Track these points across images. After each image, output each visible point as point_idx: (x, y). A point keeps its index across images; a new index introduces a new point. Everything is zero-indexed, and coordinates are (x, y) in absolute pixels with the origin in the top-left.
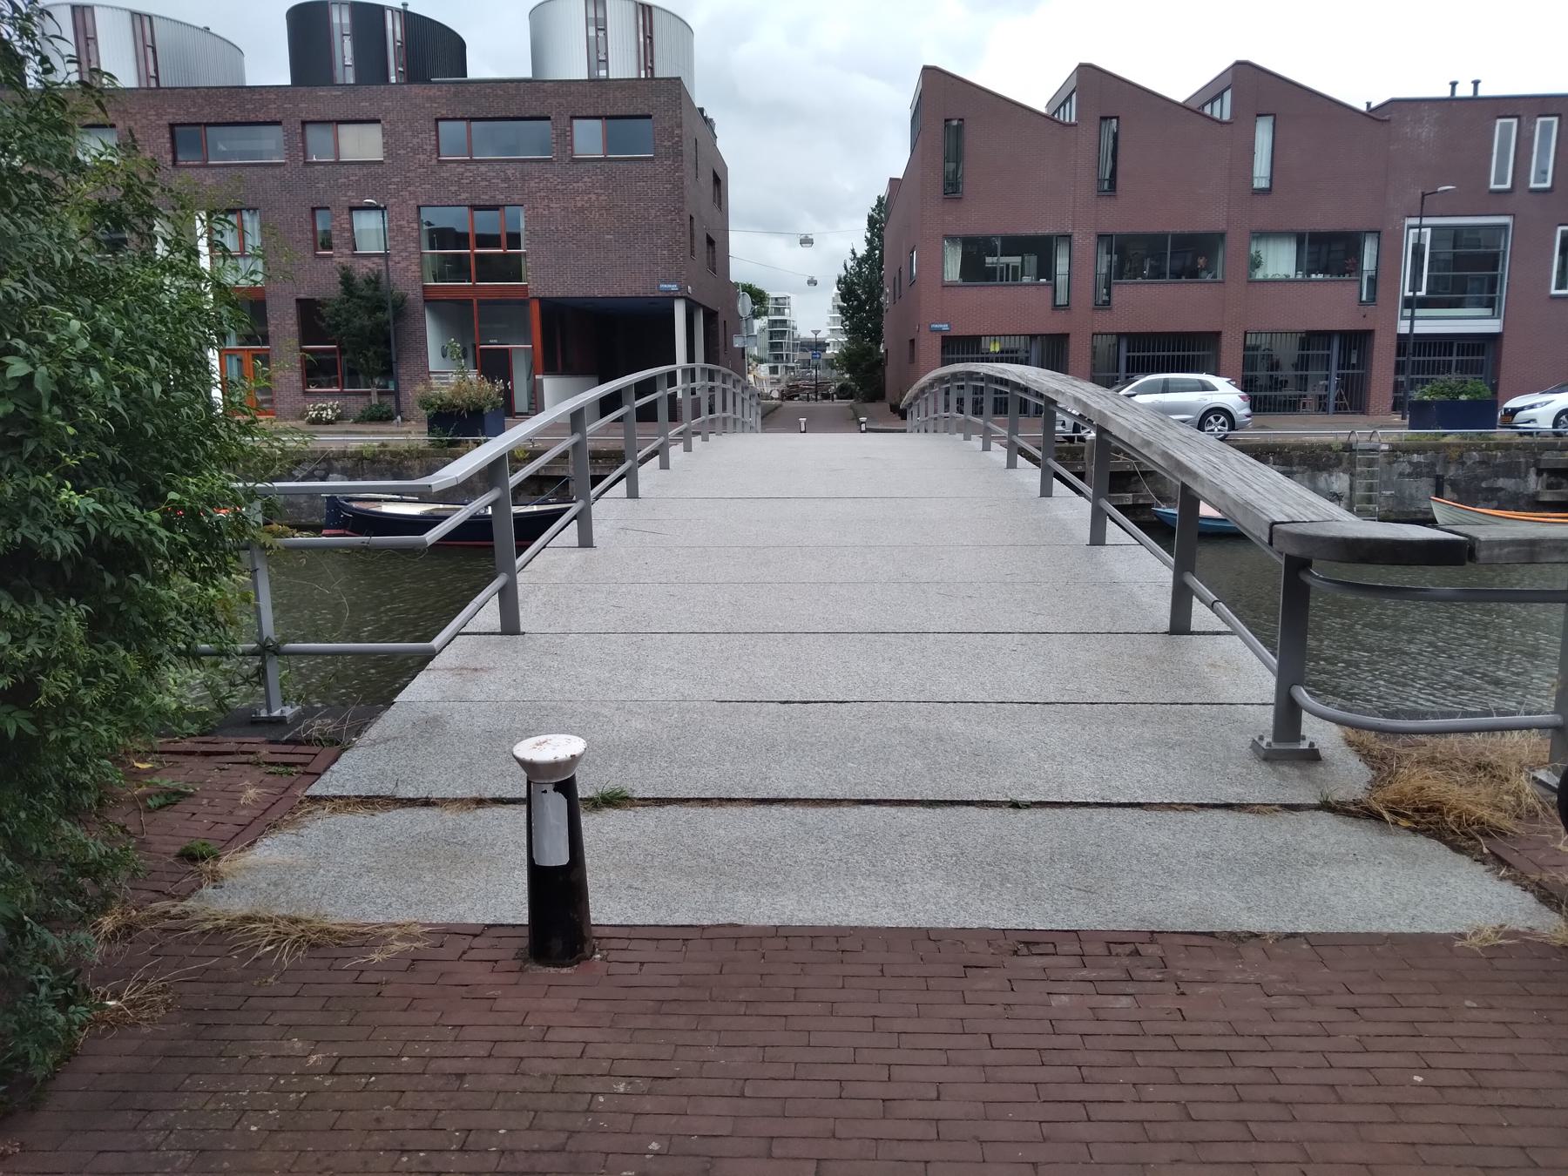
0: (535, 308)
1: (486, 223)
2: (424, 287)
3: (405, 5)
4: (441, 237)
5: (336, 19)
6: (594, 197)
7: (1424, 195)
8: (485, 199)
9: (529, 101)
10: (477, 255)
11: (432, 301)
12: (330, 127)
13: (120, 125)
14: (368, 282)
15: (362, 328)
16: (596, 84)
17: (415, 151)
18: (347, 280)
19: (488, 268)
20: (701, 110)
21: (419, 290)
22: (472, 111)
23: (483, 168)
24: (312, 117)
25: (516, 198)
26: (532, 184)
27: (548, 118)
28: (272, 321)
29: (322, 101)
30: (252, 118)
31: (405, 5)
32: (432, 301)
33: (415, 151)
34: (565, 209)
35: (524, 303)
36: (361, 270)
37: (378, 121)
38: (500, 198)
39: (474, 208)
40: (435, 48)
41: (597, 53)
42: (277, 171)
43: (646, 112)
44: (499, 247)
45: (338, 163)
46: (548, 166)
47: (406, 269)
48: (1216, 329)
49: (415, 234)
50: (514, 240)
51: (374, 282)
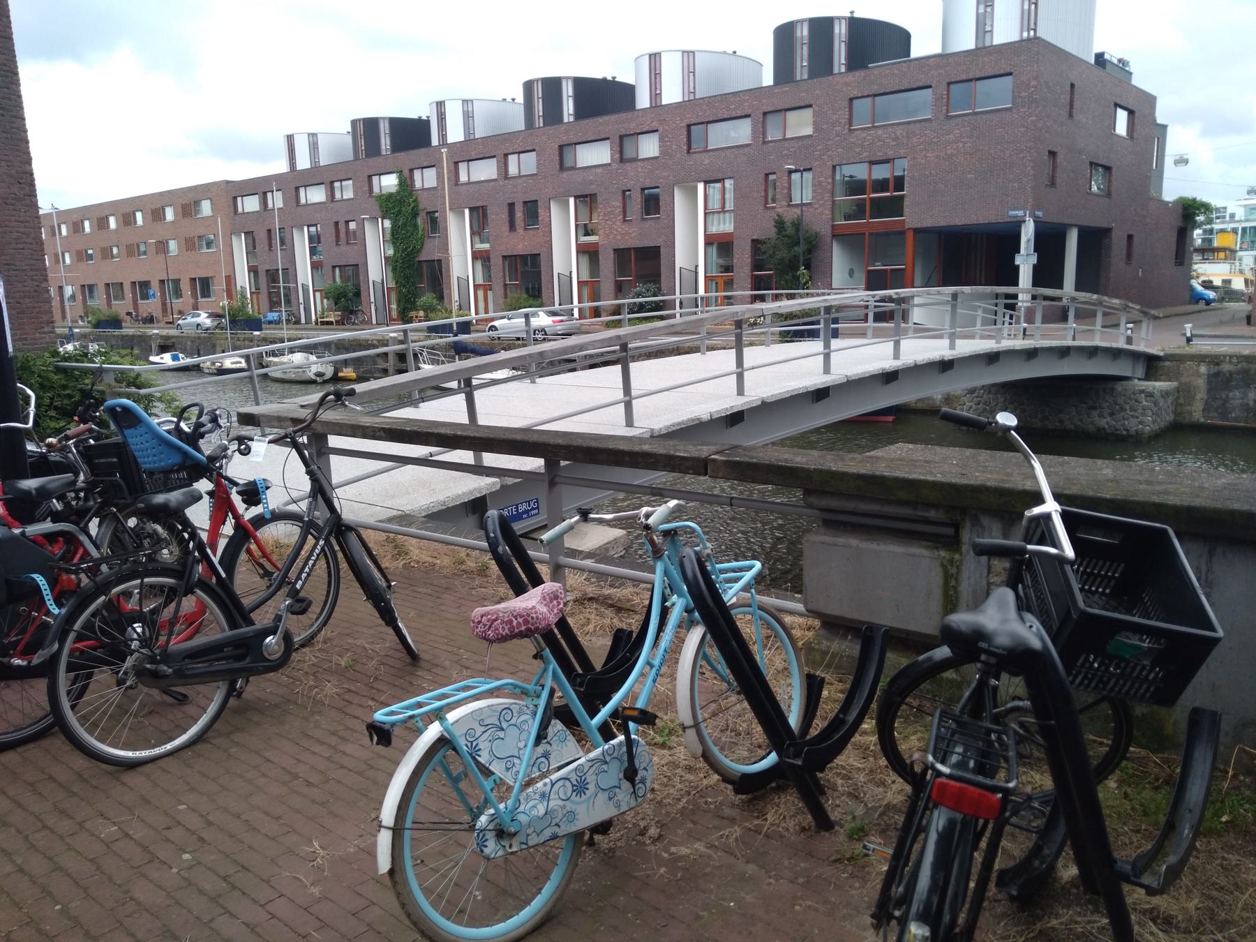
0: (910, 235)
1: (880, 173)
2: (833, 226)
3: (852, 12)
4: (855, 187)
5: (837, 30)
6: (961, 145)
7: (561, 147)
8: (880, 155)
9: (960, 73)
10: (872, 199)
11: (837, 234)
12: (781, 115)
13: (661, 129)
14: (793, 224)
15: (783, 259)
16: (983, 51)
17: (834, 125)
18: (780, 224)
19: (881, 208)
20: (1100, 58)
21: (829, 228)
22: (875, 89)
23: (880, 132)
24: (770, 109)
25: (902, 152)
26: (915, 140)
27: (930, 87)
28: (736, 256)
29: (789, 95)
30: (734, 114)
31: (852, 12)
32: (837, 234)
33: (834, 125)
34: (938, 157)
35: (902, 233)
36: (790, 215)
37: (810, 106)
38: (891, 154)
39: (872, 163)
40: (898, 39)
41: (983, 26)
42: (746, 150)
43: (1008, 70)
44: (887, 191)
45: (785, 139)
46: (927, 125)
47: (821, 214)
48: (1105, 225)
49: (829, 187)
50: (899, 183)
51: (797, 225)
